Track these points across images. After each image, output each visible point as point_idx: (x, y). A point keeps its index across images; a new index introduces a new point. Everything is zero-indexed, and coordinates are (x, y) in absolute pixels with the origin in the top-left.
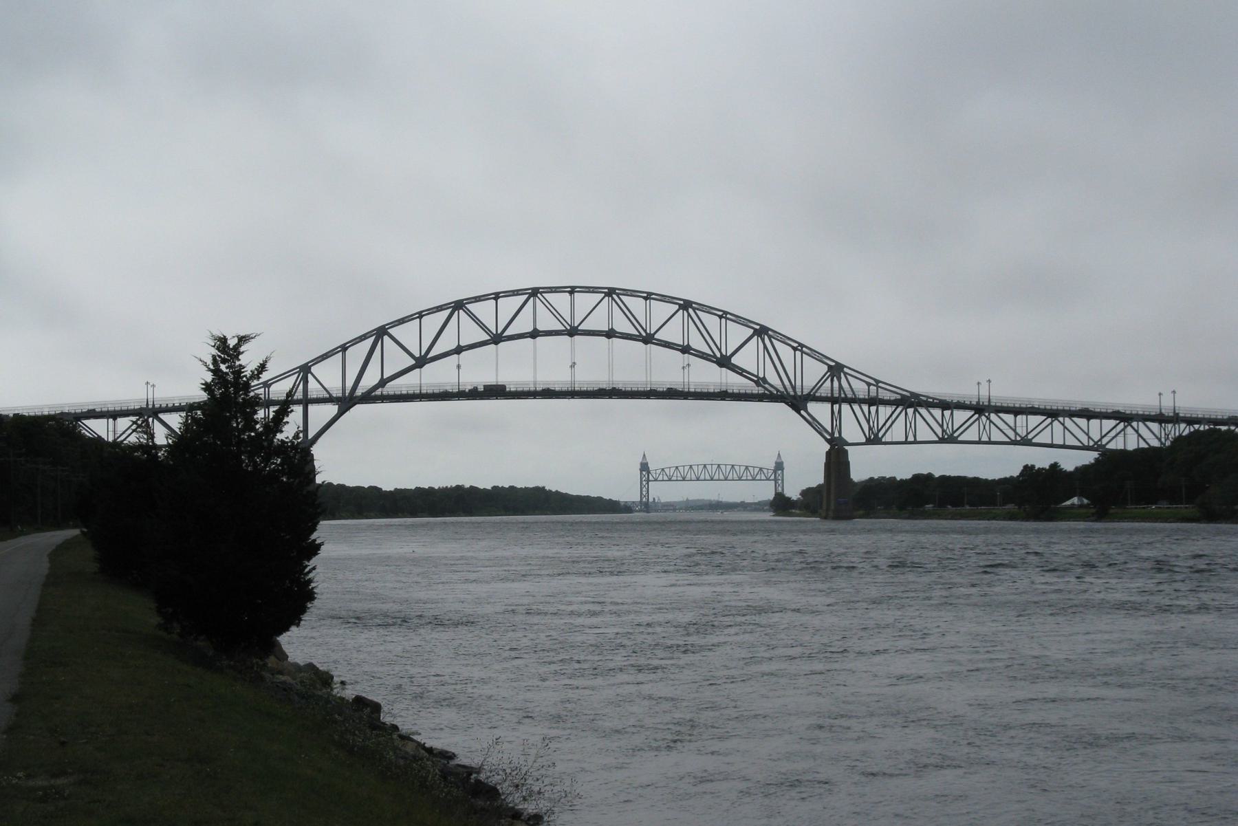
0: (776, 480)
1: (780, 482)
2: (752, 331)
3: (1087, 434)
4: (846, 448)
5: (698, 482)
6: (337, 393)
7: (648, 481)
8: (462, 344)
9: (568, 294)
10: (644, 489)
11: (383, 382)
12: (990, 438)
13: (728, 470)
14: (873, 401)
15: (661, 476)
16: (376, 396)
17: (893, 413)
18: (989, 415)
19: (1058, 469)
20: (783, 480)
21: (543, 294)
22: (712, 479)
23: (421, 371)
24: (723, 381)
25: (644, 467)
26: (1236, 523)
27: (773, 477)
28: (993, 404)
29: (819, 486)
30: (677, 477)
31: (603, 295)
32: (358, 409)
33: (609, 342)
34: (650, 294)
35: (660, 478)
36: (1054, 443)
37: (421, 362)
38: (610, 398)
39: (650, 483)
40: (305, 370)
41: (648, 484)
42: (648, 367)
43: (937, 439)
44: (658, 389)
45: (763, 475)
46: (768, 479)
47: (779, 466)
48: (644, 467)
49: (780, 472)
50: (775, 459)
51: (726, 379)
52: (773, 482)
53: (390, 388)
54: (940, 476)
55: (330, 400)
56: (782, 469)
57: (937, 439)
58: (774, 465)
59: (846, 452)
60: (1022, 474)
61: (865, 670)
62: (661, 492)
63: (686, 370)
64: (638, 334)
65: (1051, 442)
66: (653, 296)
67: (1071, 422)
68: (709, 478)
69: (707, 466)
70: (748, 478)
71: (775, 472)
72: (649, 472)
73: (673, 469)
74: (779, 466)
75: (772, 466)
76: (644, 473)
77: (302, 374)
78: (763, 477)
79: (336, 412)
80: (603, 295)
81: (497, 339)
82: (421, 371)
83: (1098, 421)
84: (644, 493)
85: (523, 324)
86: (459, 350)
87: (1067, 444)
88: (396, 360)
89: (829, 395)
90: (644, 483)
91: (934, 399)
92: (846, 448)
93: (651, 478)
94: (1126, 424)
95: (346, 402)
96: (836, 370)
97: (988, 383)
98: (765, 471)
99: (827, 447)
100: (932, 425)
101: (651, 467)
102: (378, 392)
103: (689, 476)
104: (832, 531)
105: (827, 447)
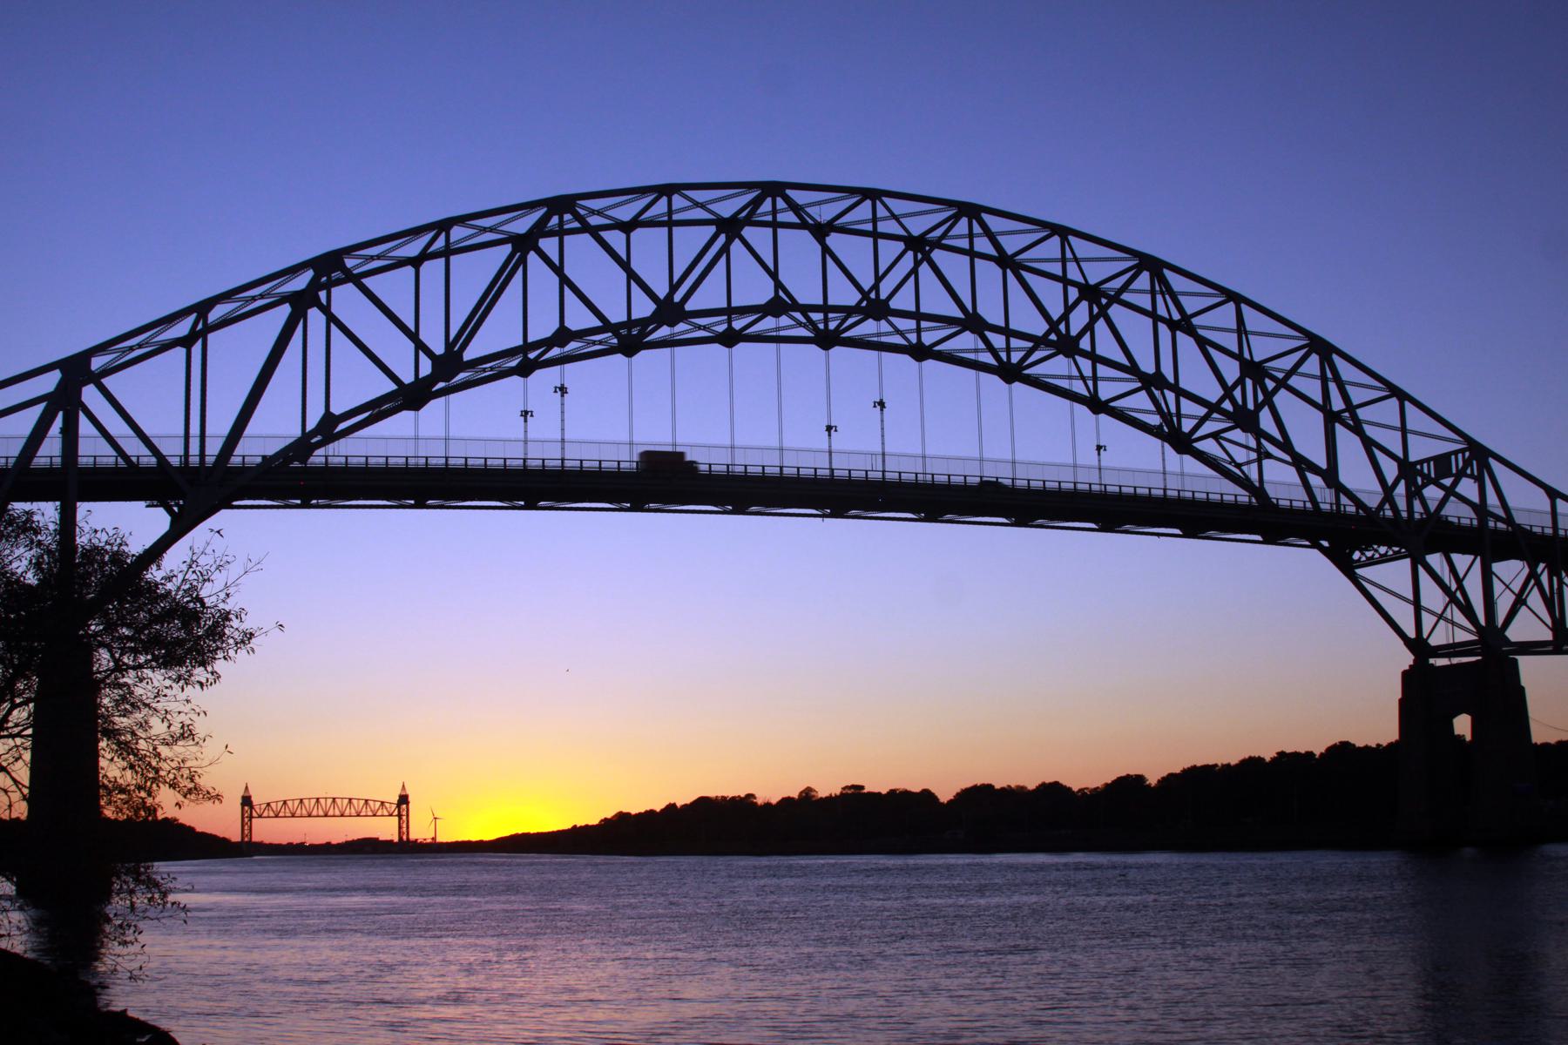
0: (400, 816)
1: (404, 818)
5: (326, 818)
7: (251, 817)
10: (246, 827)
13: (361, 805)
15: (266, 811)
17: (819, 203)
18: (1381, 507)
19: (814, 799)
20: (408, 816)
22: (342, 815)
23: (416, 420)
25: (247, 801)
27: (396, 813)
29: (1396, 741)
39: (253, 820)
41: (250, 820)
45: (385, 810)
46: (391, 815)
47: (404, 800)
48: (247, 801)
49: (404, 806)
50: (241, 793)
52: (397, 818)
54: (1329, 749)
56: (407, 803)
58: (398, 798)
60: (888, 793)
62: (266, 830)
65: (207, 454)
67: (1467, 577)
69: (321, 800)
70: (287, 815)
71: (399, 805)
73: (280, 804)
74: (404, 800)
75: (395, 799)
76: (246, 808)
78: (386, 813)
82: (416, 420)
83: (1456, 641)
84: (246, 832)
90: (246, 820)
93: (254, 814)
98: (387, 805)
101: (255, 800)
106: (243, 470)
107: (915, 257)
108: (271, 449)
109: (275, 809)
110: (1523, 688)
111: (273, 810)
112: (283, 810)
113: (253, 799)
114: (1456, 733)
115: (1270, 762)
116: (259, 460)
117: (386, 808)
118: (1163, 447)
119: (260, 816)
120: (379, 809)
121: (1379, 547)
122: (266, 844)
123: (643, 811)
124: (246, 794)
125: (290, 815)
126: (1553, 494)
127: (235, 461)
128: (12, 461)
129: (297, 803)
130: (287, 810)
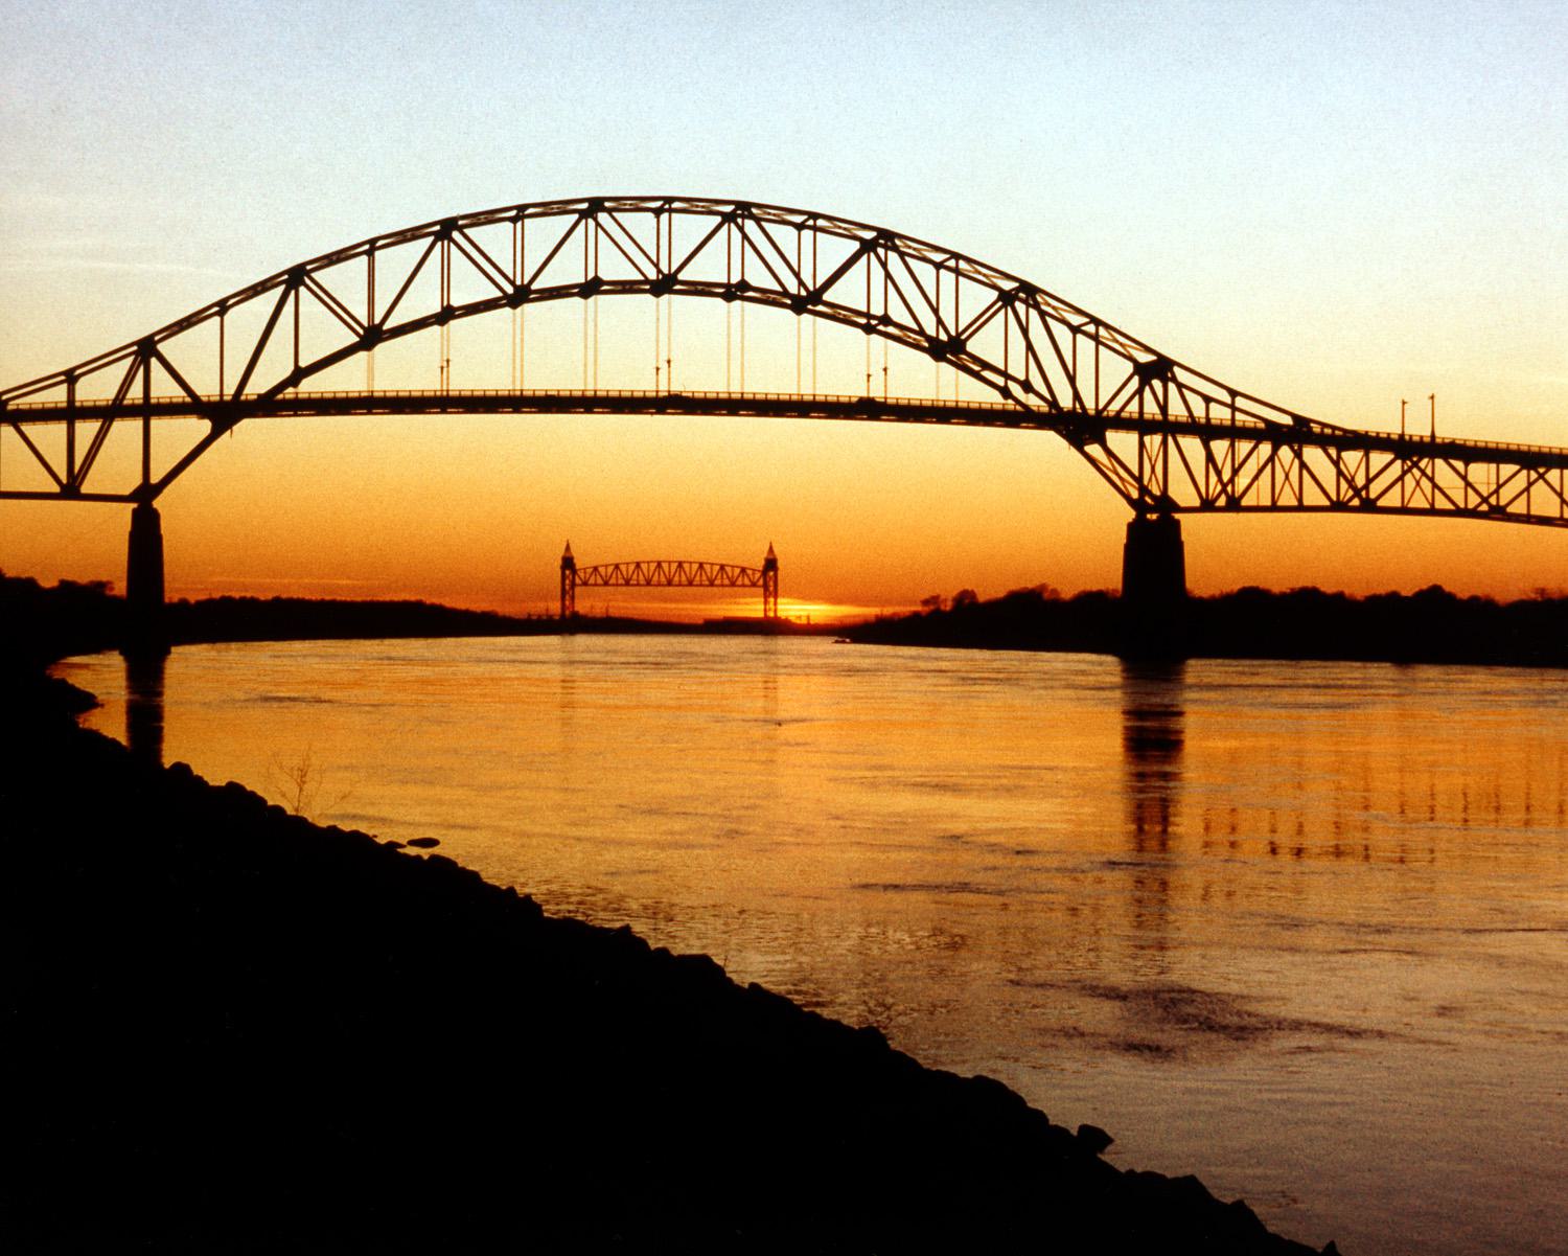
2: (995, 294)
3: (1560, 495)
4: (1177, 516)
6: (207, 389)
7: (573, 585)
8: (456, 302)
9: (651, 215)
11: (299, 374)
12: (1300, 499)
13: (673, 571)
14: (1233, 433)
16: (284, 401)
21: (615, 214)
24: (661, 388)
25: (568, 563)
26: (1552, 680)
27: (761, 582)
28: (1438, 441)
29: (121, 654)
30: (638, 580)
31: (718, 219)
32: (246, 426)
33: (586, 307)
34: (522, 208)
35: (592, 581)
36: (1533, 512)
37: (372, 336)
38: (370, 413)
40: (146, 350)
42: (518, 354)
43: (1327, 503)
44: (684, 394)
46: (754, 585)
47: (771, 564)
48: (568, 563)
49: (771, 574)
50: (561, 552)
51: (522, 385)
53: (310, 387)
55: (194, 406)
57: (1327, 503)
59: (1178, 522)
61: (1342, 947)
62: (587, 603)
63: (664, 357)
64: (779, 289)
66: (531, 211)
68: (642, 582)
71: (764, 573)
72: (574, 572)
75: (760, 564)
76: (567, 572)
77: (948, 356)
79: (209, 431)
80: (718, 219)
81: (520, 296)
85: (568, 270)
86: (446, 315)
87: (1533, 512)
88: (324, 333)
89: (1229, 423)
91: (1334, 428)
92: (1177, 516)
93: (578, 581)
94: (1533, 473)
95: (224, 414)
96: (1157, 369)
97: (1430, 401)
98: (749, 572)
99: (1131, 514)
100: (1385, 474)
101: (579, 564)
102: (290, 392)
103: (655, 578)
104: (1325, 667)
105: (1131, 514)
106: (247, 402)
107: (1368, 493)
108: (263, 391)
109: (603, 574)
110: (234, 789)
111: (601, 576)
112: (614, 576)
113: (575, 561)
114: (173, 649)
115: (172, 605)
116: (255, 397)
117: (748, 576)
118: (1293, 461)
119: (585, 584)
120: (739, 576)
121: (1467, 465)
122: (994, 605)
123: (249, 788)
124: (567, 555)
125: (707, 583)
126: (1563, 501)
127: (243, 398)
128: (110, 402)
129: (695, 566)
130: (641, 577)
